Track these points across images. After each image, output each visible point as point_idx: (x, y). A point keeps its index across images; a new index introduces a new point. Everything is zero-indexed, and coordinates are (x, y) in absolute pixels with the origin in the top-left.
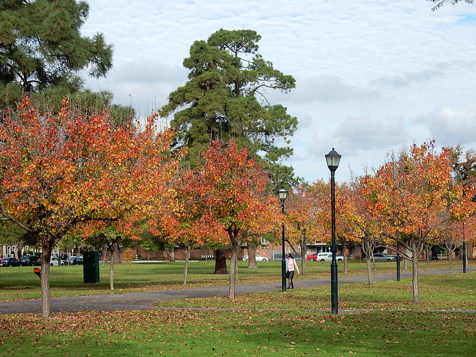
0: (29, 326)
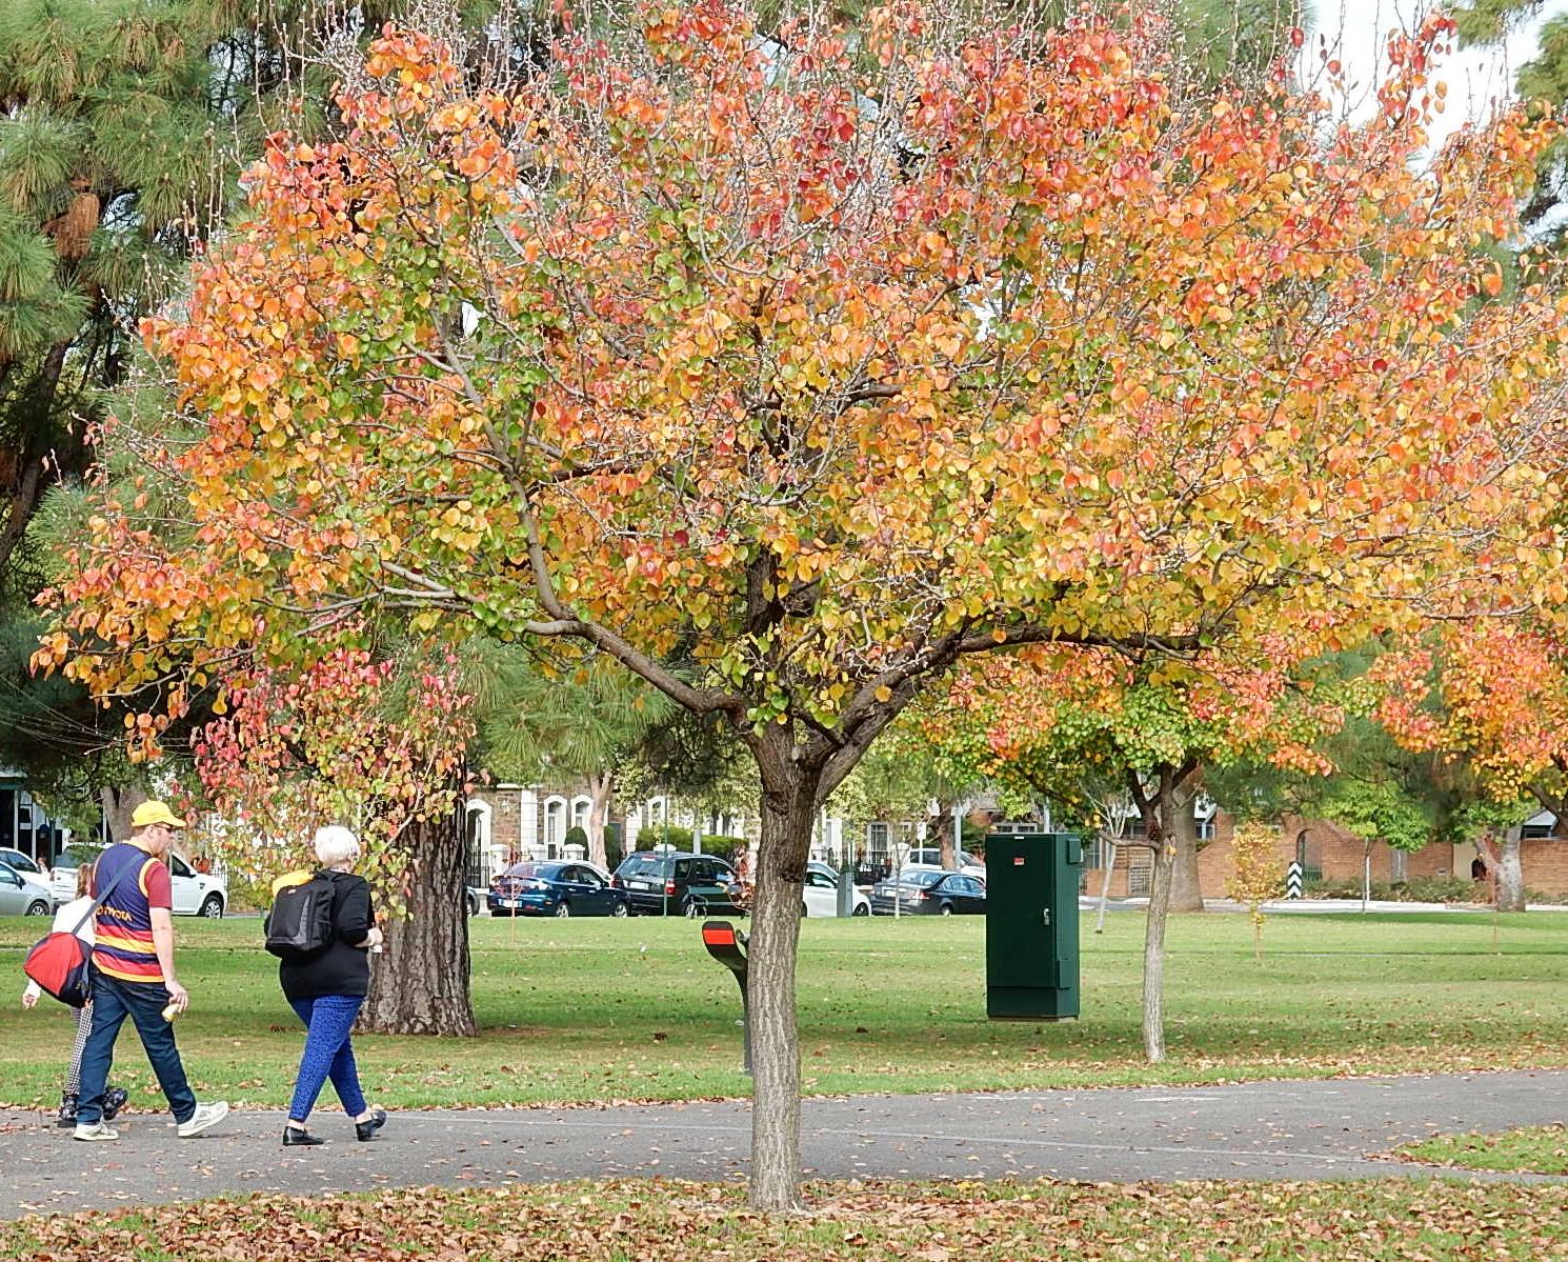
0: (677, 1252)
